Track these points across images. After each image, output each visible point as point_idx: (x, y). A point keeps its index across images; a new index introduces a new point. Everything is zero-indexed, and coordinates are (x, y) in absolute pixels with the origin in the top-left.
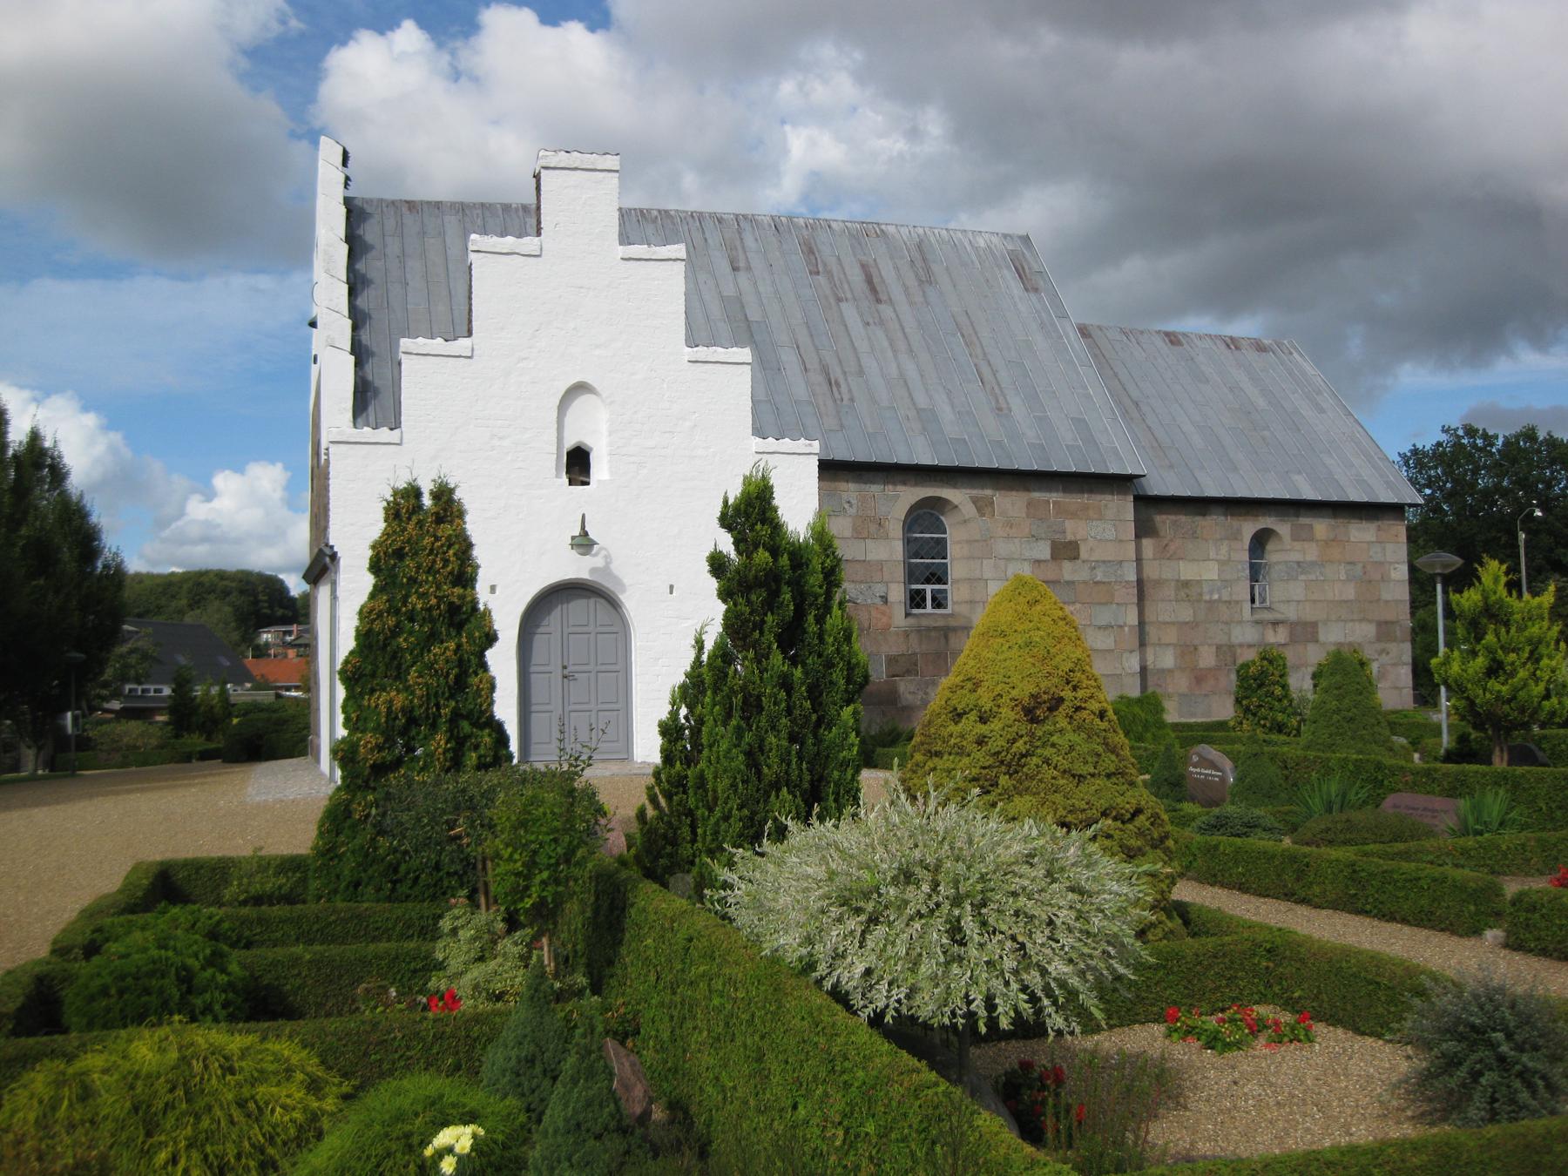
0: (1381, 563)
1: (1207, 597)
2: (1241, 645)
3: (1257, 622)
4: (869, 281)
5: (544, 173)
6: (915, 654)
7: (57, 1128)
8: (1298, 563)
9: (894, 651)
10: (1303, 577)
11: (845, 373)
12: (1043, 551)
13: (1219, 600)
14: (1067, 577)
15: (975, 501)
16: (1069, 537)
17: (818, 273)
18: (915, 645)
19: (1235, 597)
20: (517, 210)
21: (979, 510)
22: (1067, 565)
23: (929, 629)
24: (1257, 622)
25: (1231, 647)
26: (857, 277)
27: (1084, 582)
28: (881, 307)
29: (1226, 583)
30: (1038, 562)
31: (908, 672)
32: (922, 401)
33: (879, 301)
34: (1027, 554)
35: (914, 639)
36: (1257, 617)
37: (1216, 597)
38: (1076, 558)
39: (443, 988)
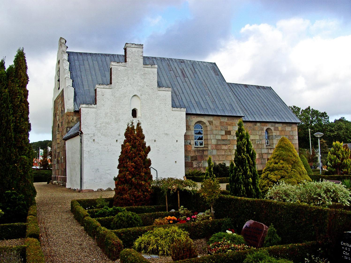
0: (292, 135)
1: (257, 143)
2: (264, 153)
3: (267, 148)
4: (182, 72)
5: (244, 124)
6: (197, 156)
7: (256, 253)
8: (275, 135)
9: (192, 155)
10: (276, 139)
11: (179, 93)
12: (223, 133)
13: (259, 144)
14: (228, 139)
15: (209, 122)
16: (229, 130)
17: (171, 71)
18: (197, 154)
19: (262, 143)
20: (104, 55)
21: (210, 124)
22: (228, 136)
23: (199, 150)
24: (267, 148)
25: (262, 154)
26: (180, 72)
27: (232, 140)
28: (185, 78)
29: (261, 140)
30: (222, 135)
31: (195, 160)
32: (197, 100)
33: (185, 77)
34: (220, 134)
35: (196, 152)
36: (267, 147)
37: (258, 143)
38: (230, 134)
39: (157, 233)
